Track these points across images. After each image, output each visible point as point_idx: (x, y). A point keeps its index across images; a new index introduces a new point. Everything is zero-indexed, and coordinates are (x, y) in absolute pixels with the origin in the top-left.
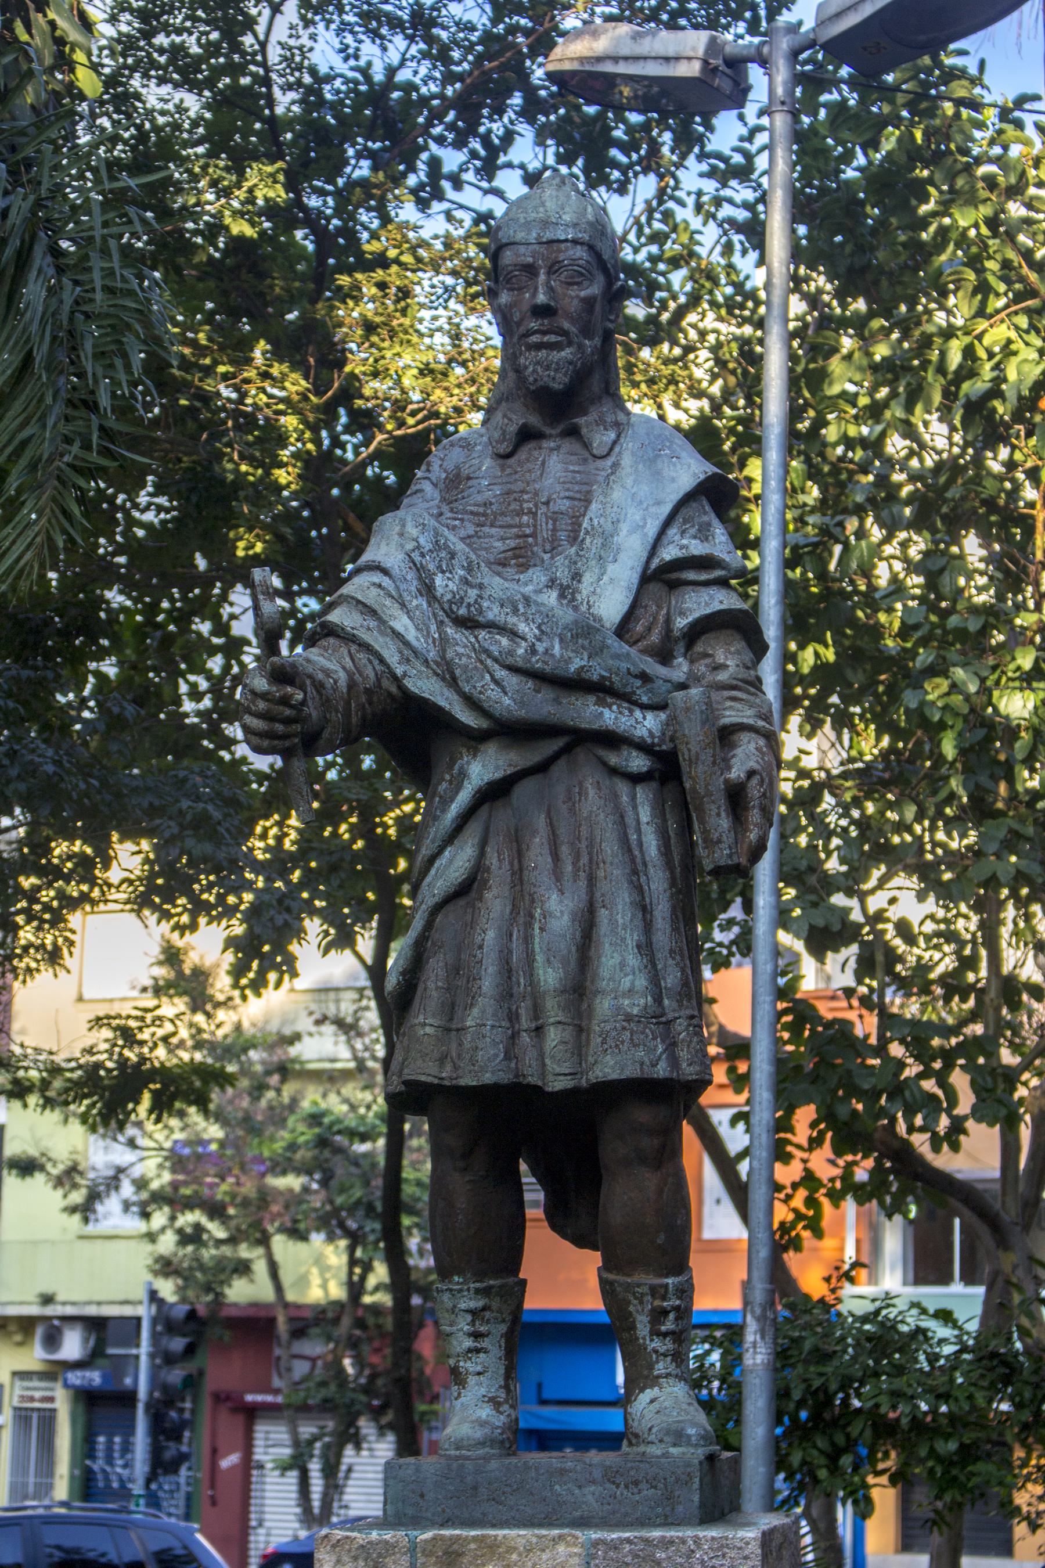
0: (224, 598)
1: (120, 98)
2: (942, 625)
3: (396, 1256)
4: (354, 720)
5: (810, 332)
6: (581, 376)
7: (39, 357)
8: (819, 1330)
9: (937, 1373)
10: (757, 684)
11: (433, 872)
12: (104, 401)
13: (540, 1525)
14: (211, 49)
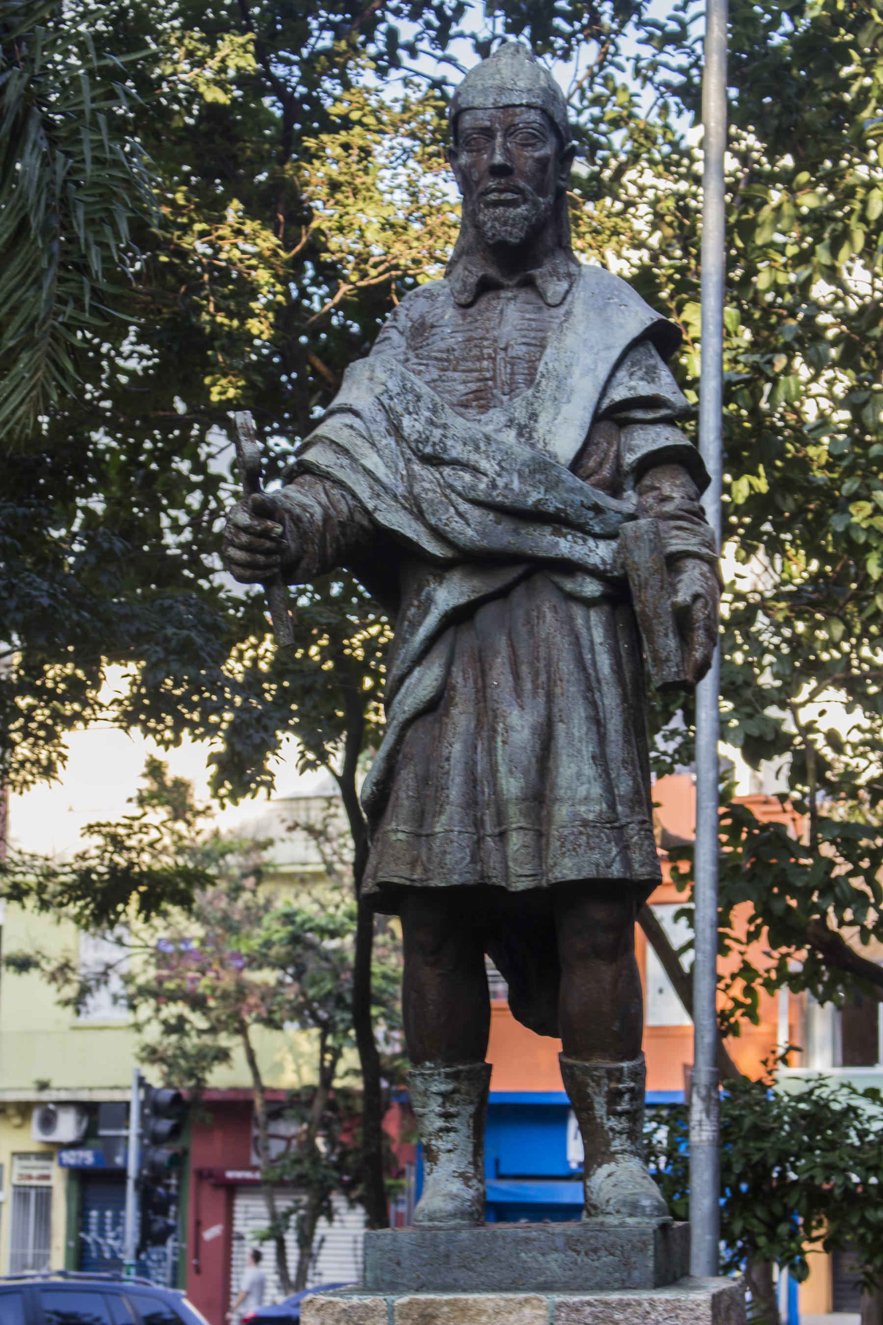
0: (201, 438)
2: (865, 455)
3: (366, 1044)
4: (329, 551)
5: (742, 186)
7: (34, 222)
8: (757, 1108)
9: (867, 1147)
10: (700, 513)
11: (403, 690)
12: (96, 265)
13: (507, 1290)
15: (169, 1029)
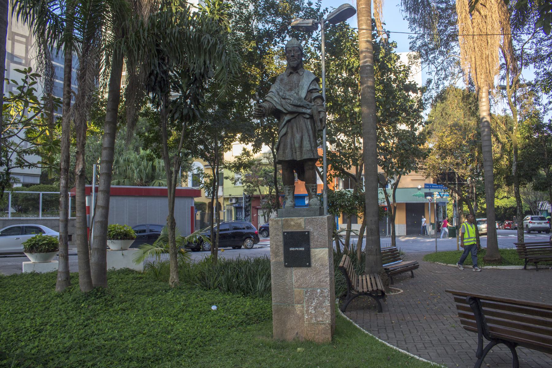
1: (233, 34)
6: (298, 65)
10: (323, 105)
12: (233, 72)
14: (245, 26)
15: (248, 187)
